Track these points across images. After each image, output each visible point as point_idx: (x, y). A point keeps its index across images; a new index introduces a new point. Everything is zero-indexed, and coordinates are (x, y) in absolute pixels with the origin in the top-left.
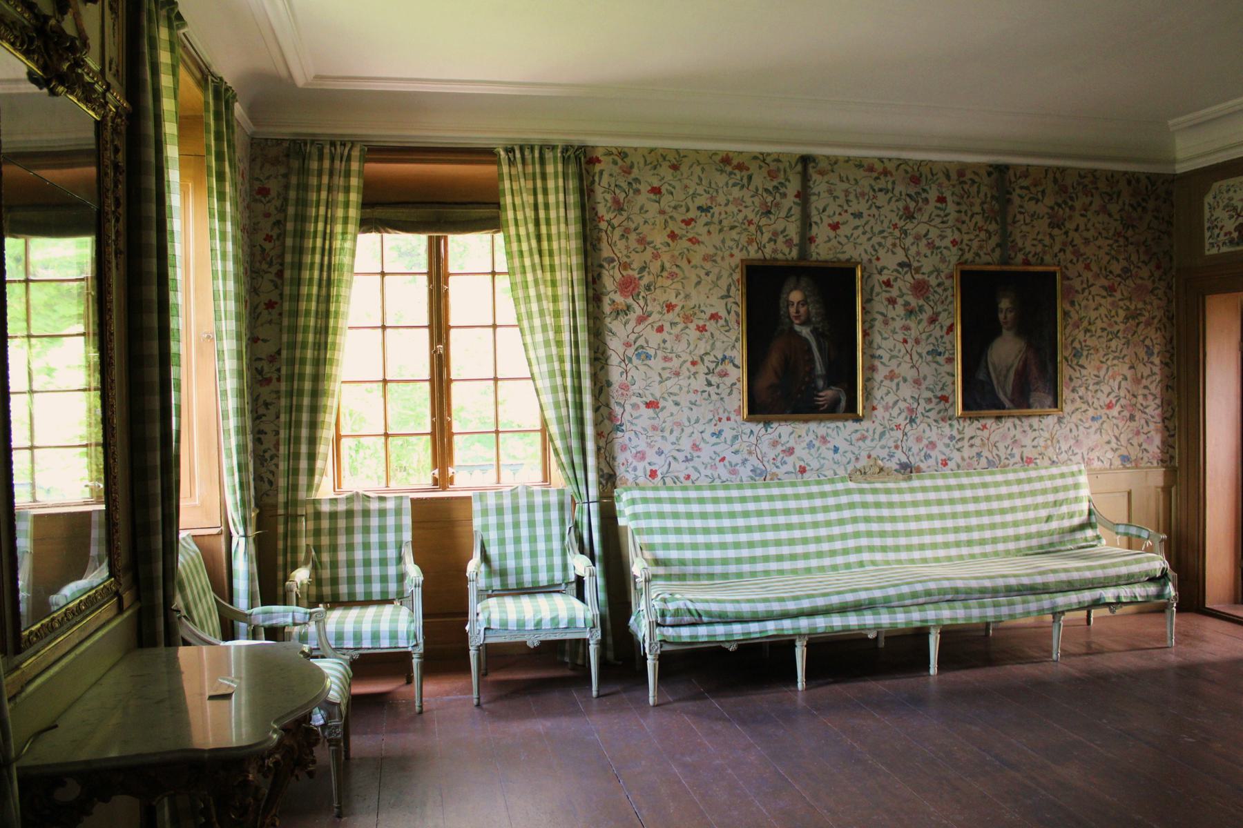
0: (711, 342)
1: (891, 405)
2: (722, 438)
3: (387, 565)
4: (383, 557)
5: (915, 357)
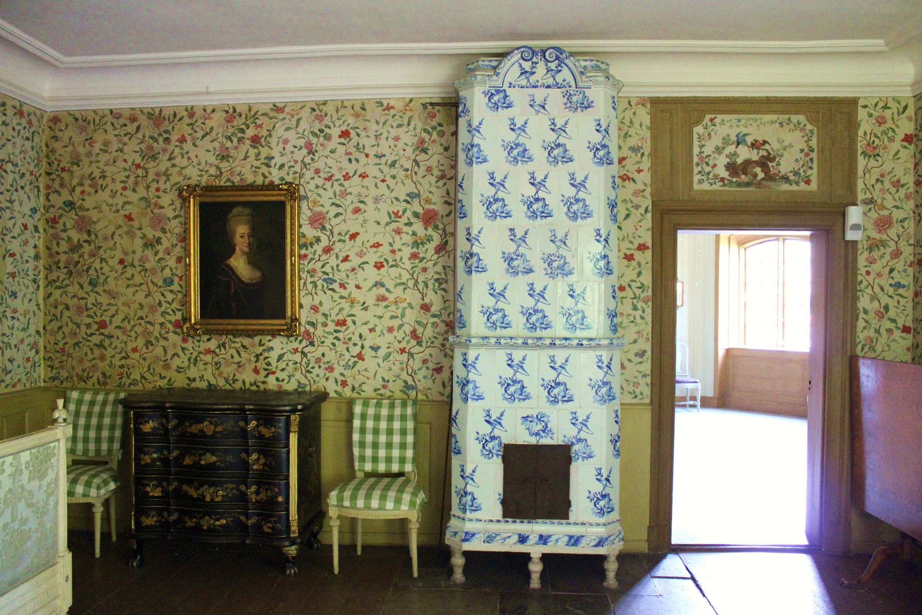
0: (637, 270)
1: (56, 329)
2: (645, 358)
3: (400, 458)
4: (389, 450)
5: (877, 289)
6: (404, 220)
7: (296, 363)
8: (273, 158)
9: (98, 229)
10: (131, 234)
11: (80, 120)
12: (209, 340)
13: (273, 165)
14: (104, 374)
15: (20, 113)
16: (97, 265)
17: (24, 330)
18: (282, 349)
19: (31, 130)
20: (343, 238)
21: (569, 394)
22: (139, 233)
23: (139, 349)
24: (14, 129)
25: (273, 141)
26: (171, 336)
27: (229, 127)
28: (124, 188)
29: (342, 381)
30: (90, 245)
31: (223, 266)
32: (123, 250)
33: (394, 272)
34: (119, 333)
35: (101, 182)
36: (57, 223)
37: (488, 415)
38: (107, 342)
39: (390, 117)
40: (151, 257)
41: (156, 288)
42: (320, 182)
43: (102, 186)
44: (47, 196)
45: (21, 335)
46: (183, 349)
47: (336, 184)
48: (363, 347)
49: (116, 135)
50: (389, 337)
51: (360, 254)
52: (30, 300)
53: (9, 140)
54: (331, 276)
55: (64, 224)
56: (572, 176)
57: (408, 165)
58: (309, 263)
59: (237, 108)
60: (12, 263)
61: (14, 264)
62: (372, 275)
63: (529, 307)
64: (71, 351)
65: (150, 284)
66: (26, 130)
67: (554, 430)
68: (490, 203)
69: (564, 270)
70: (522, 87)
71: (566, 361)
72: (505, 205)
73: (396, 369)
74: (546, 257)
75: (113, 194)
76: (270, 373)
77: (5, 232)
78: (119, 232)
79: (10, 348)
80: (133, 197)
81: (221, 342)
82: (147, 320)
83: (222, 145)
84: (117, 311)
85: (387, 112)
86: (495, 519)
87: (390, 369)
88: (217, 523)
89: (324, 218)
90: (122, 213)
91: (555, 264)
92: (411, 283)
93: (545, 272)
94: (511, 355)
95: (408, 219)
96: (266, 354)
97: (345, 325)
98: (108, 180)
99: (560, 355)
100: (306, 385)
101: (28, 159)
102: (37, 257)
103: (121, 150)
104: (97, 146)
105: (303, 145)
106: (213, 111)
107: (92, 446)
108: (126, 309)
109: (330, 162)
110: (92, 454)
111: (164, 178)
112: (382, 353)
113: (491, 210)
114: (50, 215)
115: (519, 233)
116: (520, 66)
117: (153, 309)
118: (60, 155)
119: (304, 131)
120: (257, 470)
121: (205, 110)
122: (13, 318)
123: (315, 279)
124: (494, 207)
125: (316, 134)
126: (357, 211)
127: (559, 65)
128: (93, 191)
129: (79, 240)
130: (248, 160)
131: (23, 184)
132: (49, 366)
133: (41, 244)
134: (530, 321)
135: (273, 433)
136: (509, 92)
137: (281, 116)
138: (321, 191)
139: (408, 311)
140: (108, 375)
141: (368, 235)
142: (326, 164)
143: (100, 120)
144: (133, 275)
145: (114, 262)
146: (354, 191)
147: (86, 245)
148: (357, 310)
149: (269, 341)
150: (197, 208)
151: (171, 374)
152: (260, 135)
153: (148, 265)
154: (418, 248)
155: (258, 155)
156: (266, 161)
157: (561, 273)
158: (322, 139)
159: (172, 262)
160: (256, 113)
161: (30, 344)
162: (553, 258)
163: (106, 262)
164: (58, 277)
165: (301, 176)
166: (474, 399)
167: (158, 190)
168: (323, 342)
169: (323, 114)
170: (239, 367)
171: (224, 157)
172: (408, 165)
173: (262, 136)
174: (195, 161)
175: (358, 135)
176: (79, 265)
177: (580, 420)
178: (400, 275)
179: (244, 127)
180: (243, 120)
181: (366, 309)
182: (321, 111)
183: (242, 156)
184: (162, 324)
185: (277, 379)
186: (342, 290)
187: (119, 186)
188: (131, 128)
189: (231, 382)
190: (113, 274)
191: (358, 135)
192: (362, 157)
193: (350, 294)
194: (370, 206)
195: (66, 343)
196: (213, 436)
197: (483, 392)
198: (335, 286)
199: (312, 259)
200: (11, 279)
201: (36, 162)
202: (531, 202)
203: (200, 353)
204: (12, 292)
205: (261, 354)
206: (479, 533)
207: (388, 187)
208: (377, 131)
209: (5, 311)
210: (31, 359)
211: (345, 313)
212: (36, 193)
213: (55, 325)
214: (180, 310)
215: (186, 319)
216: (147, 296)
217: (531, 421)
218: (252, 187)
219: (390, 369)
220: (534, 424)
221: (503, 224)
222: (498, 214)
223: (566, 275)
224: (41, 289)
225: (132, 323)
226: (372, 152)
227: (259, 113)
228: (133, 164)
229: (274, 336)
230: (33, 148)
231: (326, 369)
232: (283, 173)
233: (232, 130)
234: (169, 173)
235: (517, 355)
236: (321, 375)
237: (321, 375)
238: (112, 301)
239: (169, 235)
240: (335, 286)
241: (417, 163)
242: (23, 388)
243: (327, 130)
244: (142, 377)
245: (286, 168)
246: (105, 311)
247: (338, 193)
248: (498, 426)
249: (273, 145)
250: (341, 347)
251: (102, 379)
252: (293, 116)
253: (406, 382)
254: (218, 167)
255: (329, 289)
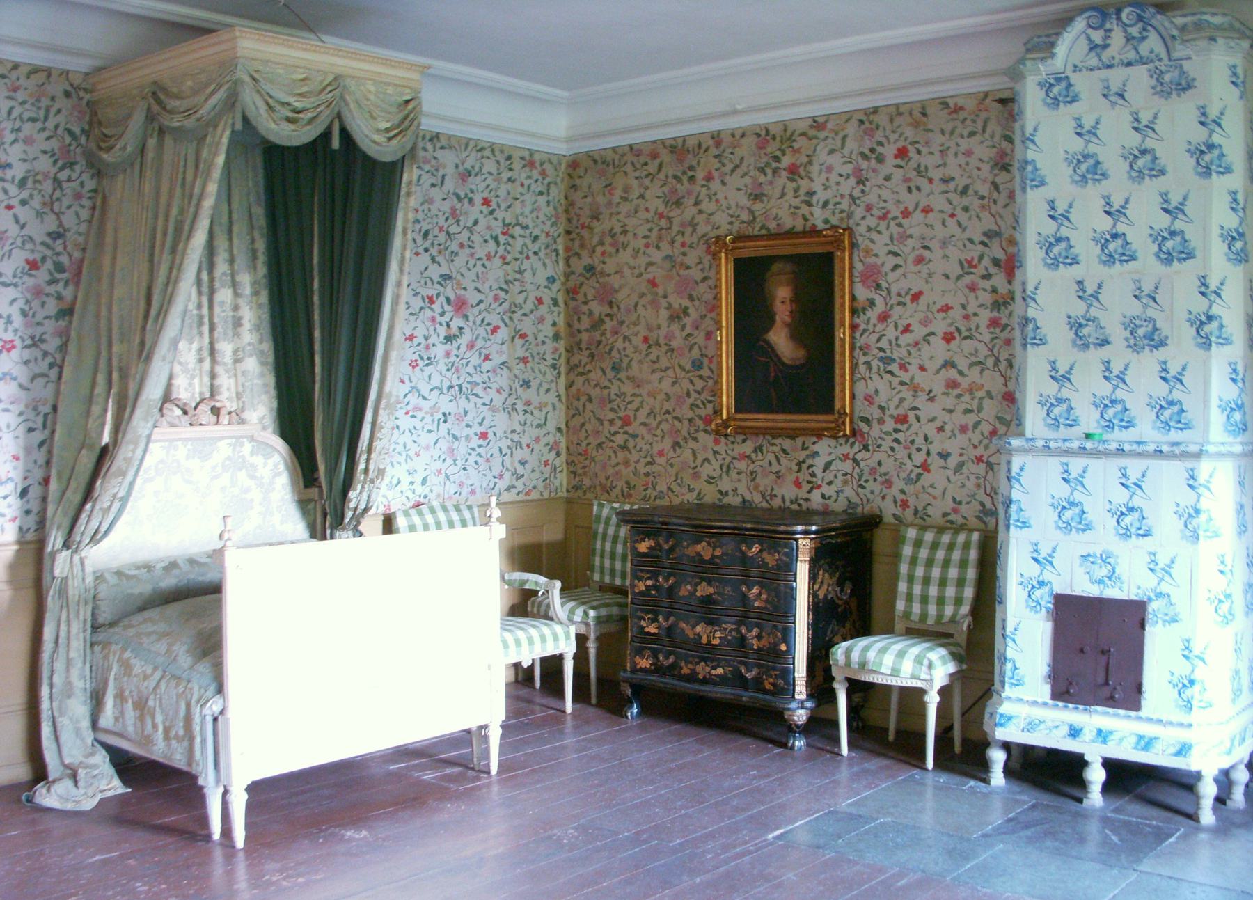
6: (980, 270)
7: (846, 474)
8: (814, 193)
9: (620, 299)
10: (654, 304)
11: (600, 162)
12: (744, 441)
13: (814, 204)
14: (628, 483)
15: (531, 164)
16: (620, 344)
17: (539, 426)
18: (830, 454)
19: (546, 182)
20: (902, 300)
21: (1146, 524)
22: (664, 303)
23: (666, 452)
24: (522, 185)
25: (815, 169)
26: (701, 436)
27: (762, 155)
28: (647, 246)
29: (902, 501)
30: (612, 320)
31: (761, 343)
32: (648, 325)
33: (968, 346)
34: (643, 431)
35: (621, 238)
36: (577, 293)
37: (1036, 551)
38: (631, 444)
39: (958, 123)
40: (677, 333)
41: (683, 373)
42: (872, 222)
43: (623, 244)
44: (567, 260)
45: (538, 432)
46: (715, 453)
47: (892, 223)
48: (928, 453)
49: (637, 178)
50: (961, 440)
51: (925, 322)
52: (548, 391)
53: (517, 199)
54: (888, 354)
55: (585, 294)
56: (1165, 197)
57: (984, 189)
58: (862, 335)
59: (770, 128)
60: (523, 346)
61: (526, 347)
62: (939, 351)
63: (1104, 394)
64: (594, 453)
65: (678, 370)
66: (539, 183)
67: (1124, 578)
68: (1051, 244)
69: (1153, 340)
70: (1091, 70)
71: (1143, 476)
72: (1071, 247)
73: (970, 485)
74: (1127, 320)
75: (636, 252)
76: (814, 487)
77: (514, 309)
78: (642, 302)
79: (521, 447)
80: (657, 256)
81: (757, 444)
82: (674, 415)
83: (754, 179)
84: (642, 403)
85: (955, 116)
86: (1040, 700)
87: (963, 486)
88: (713, 672)
89: (879, 272)
90: (646, 276)
91: (1141, 332)
92: (990, 362)
93: (1126, 344)
94: (1067, 464)
95: (986, 269)
96: (809, 462)
97: (906, 422)
98: (630, 235)
99: (1135, 468)
100: (857, 505)
101: (542, 218)
102: (556, 337)
103: (642, 196)
104: (618, 193)
105: (850, 172)
106: (743, 136)
107: (932, 609)
108: (650, 401)
109: (885, 194)
110: (931, 621)
111: (690, 229)
112: (953, 461)
113: (1107, 251)
114: (571, 284)
115: (1090, 288)
116: (1089, 38)
117: (680, 400)
118: (580, 208)
119: (851, 153)
120: (758, 608)
121: (733, 136)
122: (526, 412)
123: (868, 358)
124: (1056, 250)
125: (866, 156)
126: (920, 260)
127: (1144, 29)
128: (613, 250)
129: (600, 315)
130: (786, 198)
131: (536, 249)
132: (572, 472)
133: (561, 321)
134: (1106, 416)
135: (777, 560)
136: (1074, 78)
137: (822, 135)
138: (874, 235)
139: (987, 403)
140: (632, 484)
141: (936, 294)
142: (880, 196)
143: (620, 160)
144: (658, 356)
145: (637, 341)
146: (915, 231)
147: (607, 319)
148: (921, 401)
149: (814, 443)
150: (731, 265)
151: (700, 485)
152: (798, 163)
153: (674, 344)
154: (999, 311)
155: (796, 190)
156: (807, 198)
157: (1148, 345)
158: (873, 162)
159: (700, 338)
160: (792, 134)
161: (548, 444)
162: (1138, 322)
163: (630, 341)
164: (580, 361)
165: (850, 216)
166: (1017, 526)
167: (683, 245)
168: (879, 446)
169: (874, 126)
170: (778, 477)
171: (757, 197)
172: (984, 189)
173: (801, 165)
174: (724, 202)
175: (919, 152)
176: (601, 347)
177: (1161, 565)
178: (976, 351)
179: (778, 153)
180: (776, 144)
181: (932, 399)
182: (871, 123)
183: (777, 193)
184: (690, 420)
185: (823, 496)
186: (902, 373)
187: (641, 243)
188: (653, 167)
189: (768, 498)
190: (636, 357)
191: (919, 152)
192: (923, 183)
193: (912, 379)
194: (936, 254)
195: (589, 444)
196: (711, 561)
197: (1029, 518)
198: (894, 367)
199: (865, 330)
200: (522, 365)
201: (553, 220)
202: (1107, 240)
203: (734, 458)
204: (524, 380)
205: (804, 462)
206: (1017, 717)
207: (959, 225)
208: (942, 145)
209: (514, 404)
210: (550, 462)
211: (906, 404)
212: (554, 258)
213: (577, 421)
214: (710, 402)
215: (717, 412)
216: (674, 383)
217: (1092, 563)
218: (790, 234)
219: (963, 486)
220: (1096, 566)
221: (1068, 274)
222: (1061, 260)
223: (1156, 347)
224: (563, 376)
225: (658, 419)
226: (936, 174)
227: (797, 133)
228: (656, 214)
229: (820, 436)
230: (548, 203)
231: (883, 483)
232: (827, 214)
233: (765, 160)
234: (695, 221)
235: (1076, 465)
236: (877, 492)
237: (877, 492)
238: (637, 391)
239: (697, 303)
240: (894, 367)
241: (995, 186)
242: (539, 497)
243: (880, 149)
244: (669, 488)
245: (830, 206)
246: (629, 403)
247: (895, 236)
248: (1049, 567)
249: (814, 175)
250: (901, 453)
251: (626, 490)
252: (836, 134)
253: (982, 504)
254: (751, 211)
255: (887, 372)
